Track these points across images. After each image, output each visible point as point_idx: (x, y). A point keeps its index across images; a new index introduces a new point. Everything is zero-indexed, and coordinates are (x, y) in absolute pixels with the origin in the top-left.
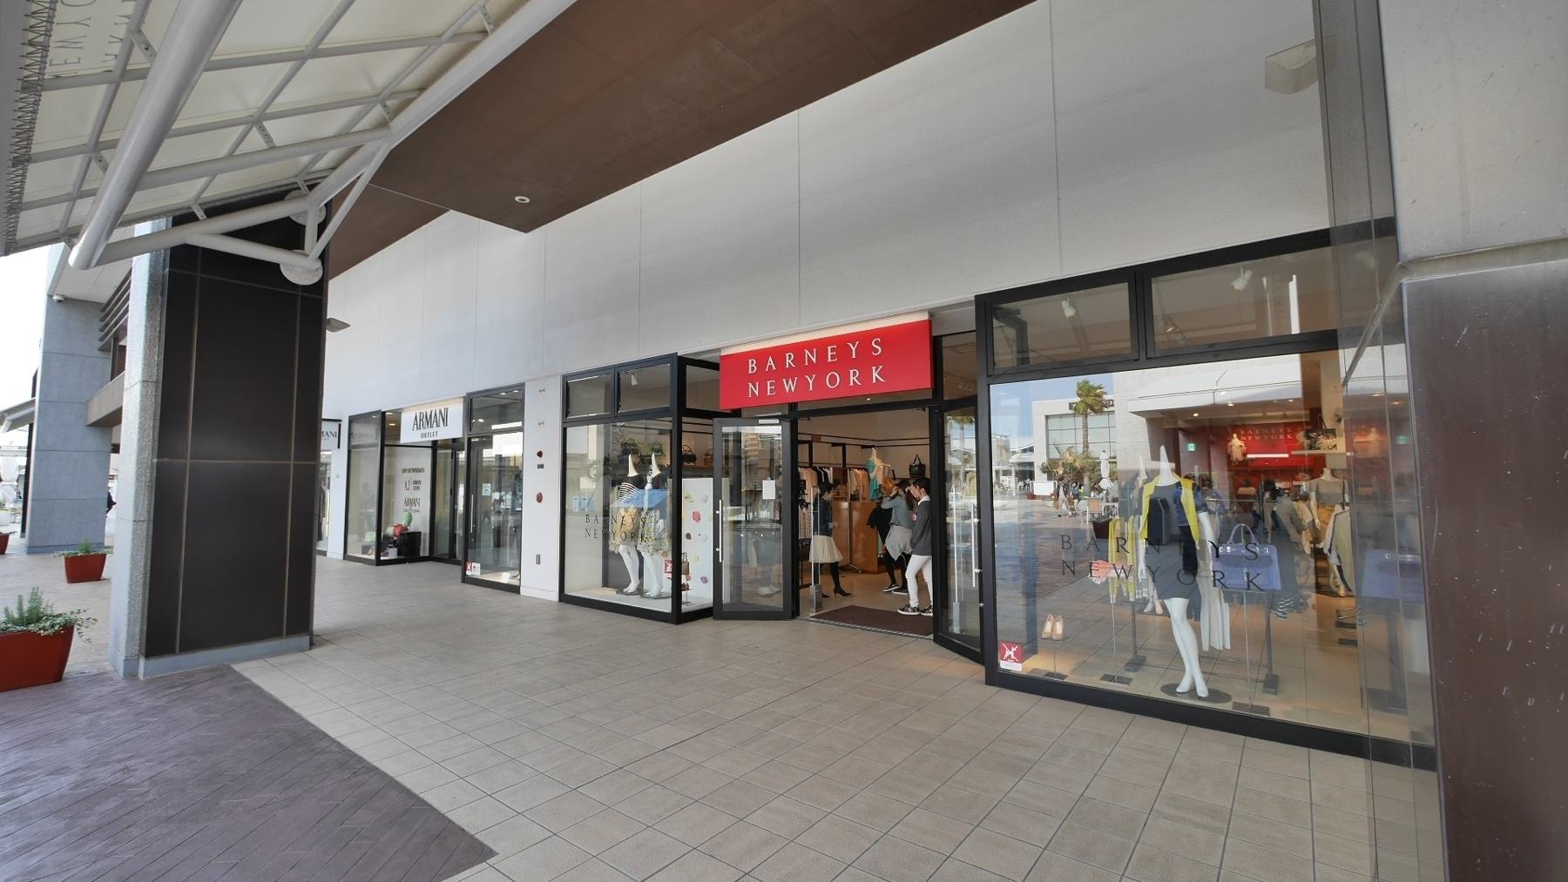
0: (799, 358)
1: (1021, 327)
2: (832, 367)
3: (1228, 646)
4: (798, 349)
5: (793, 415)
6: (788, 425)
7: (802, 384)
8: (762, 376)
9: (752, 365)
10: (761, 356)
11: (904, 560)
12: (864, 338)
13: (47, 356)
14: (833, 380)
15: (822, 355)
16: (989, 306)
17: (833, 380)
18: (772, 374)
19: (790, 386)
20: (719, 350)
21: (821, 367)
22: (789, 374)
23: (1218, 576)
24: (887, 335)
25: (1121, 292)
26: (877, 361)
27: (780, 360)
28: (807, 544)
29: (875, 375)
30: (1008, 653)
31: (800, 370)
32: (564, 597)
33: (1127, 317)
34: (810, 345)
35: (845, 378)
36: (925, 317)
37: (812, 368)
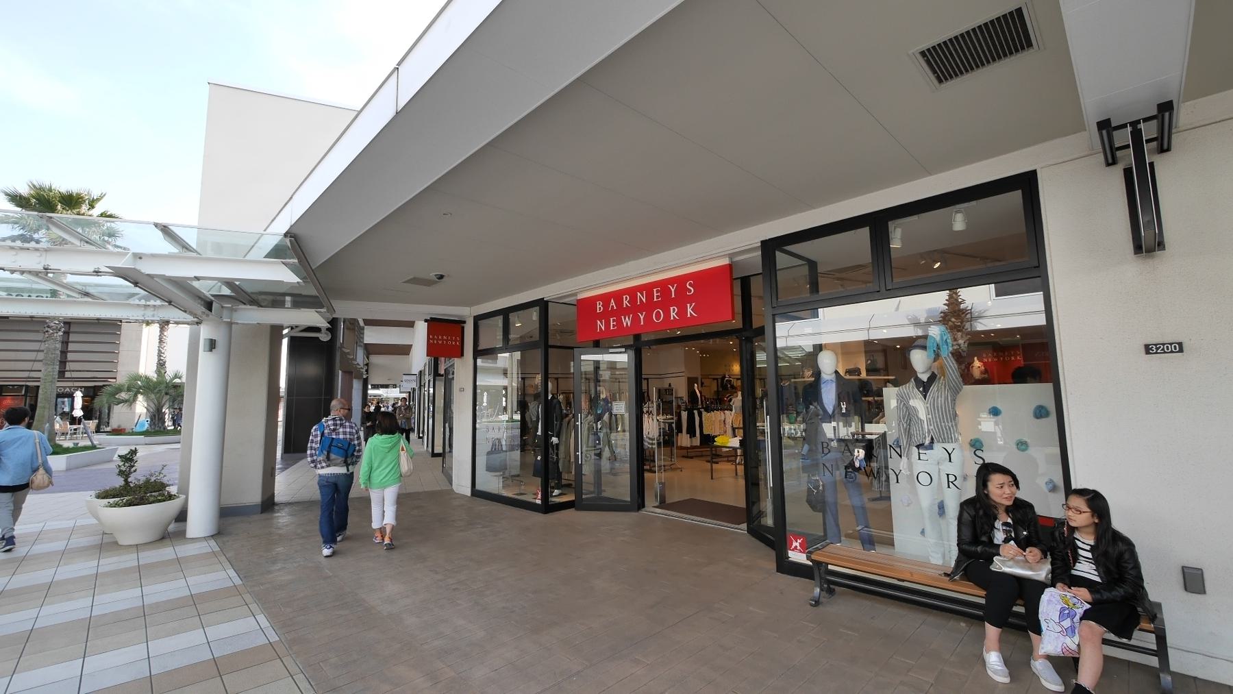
0: (633, 299)
1: (812, 265)
2: (657, 305)
3: (1074, 572)
4: (632, 292)
5: (637, 347)
6: (632, 353)
7: (636, 320)
8: (606, 315)
9: (599, 307)
10: (605, 298)
11: (1006, 541)
12: (680, 281)
13: (1143, 588)
14: (658, 315)
15: (650, 296)
16: (770, 247)
17: (658, 315)
18: (613, 313)
19: (627, 321)
20: (575, 294)
21: (649, 306)
22: (626, 312)
23: (952, 478)
24: (698, 277)
25: (864, 233)
26: (690, 299)
27: (619, 302)
28: (995, 550)
29: (689, 310)
30: (795, 544)
31: (634, 309)
32: (476, 493)
33: (1024, 229)
34: (640, 288)
35: (667, 314)
36: (726, 261)
37: (642, 307)
